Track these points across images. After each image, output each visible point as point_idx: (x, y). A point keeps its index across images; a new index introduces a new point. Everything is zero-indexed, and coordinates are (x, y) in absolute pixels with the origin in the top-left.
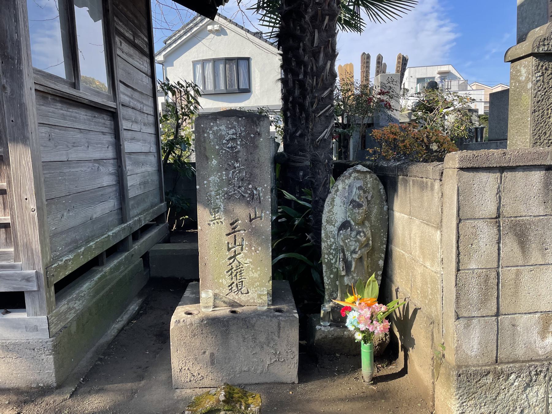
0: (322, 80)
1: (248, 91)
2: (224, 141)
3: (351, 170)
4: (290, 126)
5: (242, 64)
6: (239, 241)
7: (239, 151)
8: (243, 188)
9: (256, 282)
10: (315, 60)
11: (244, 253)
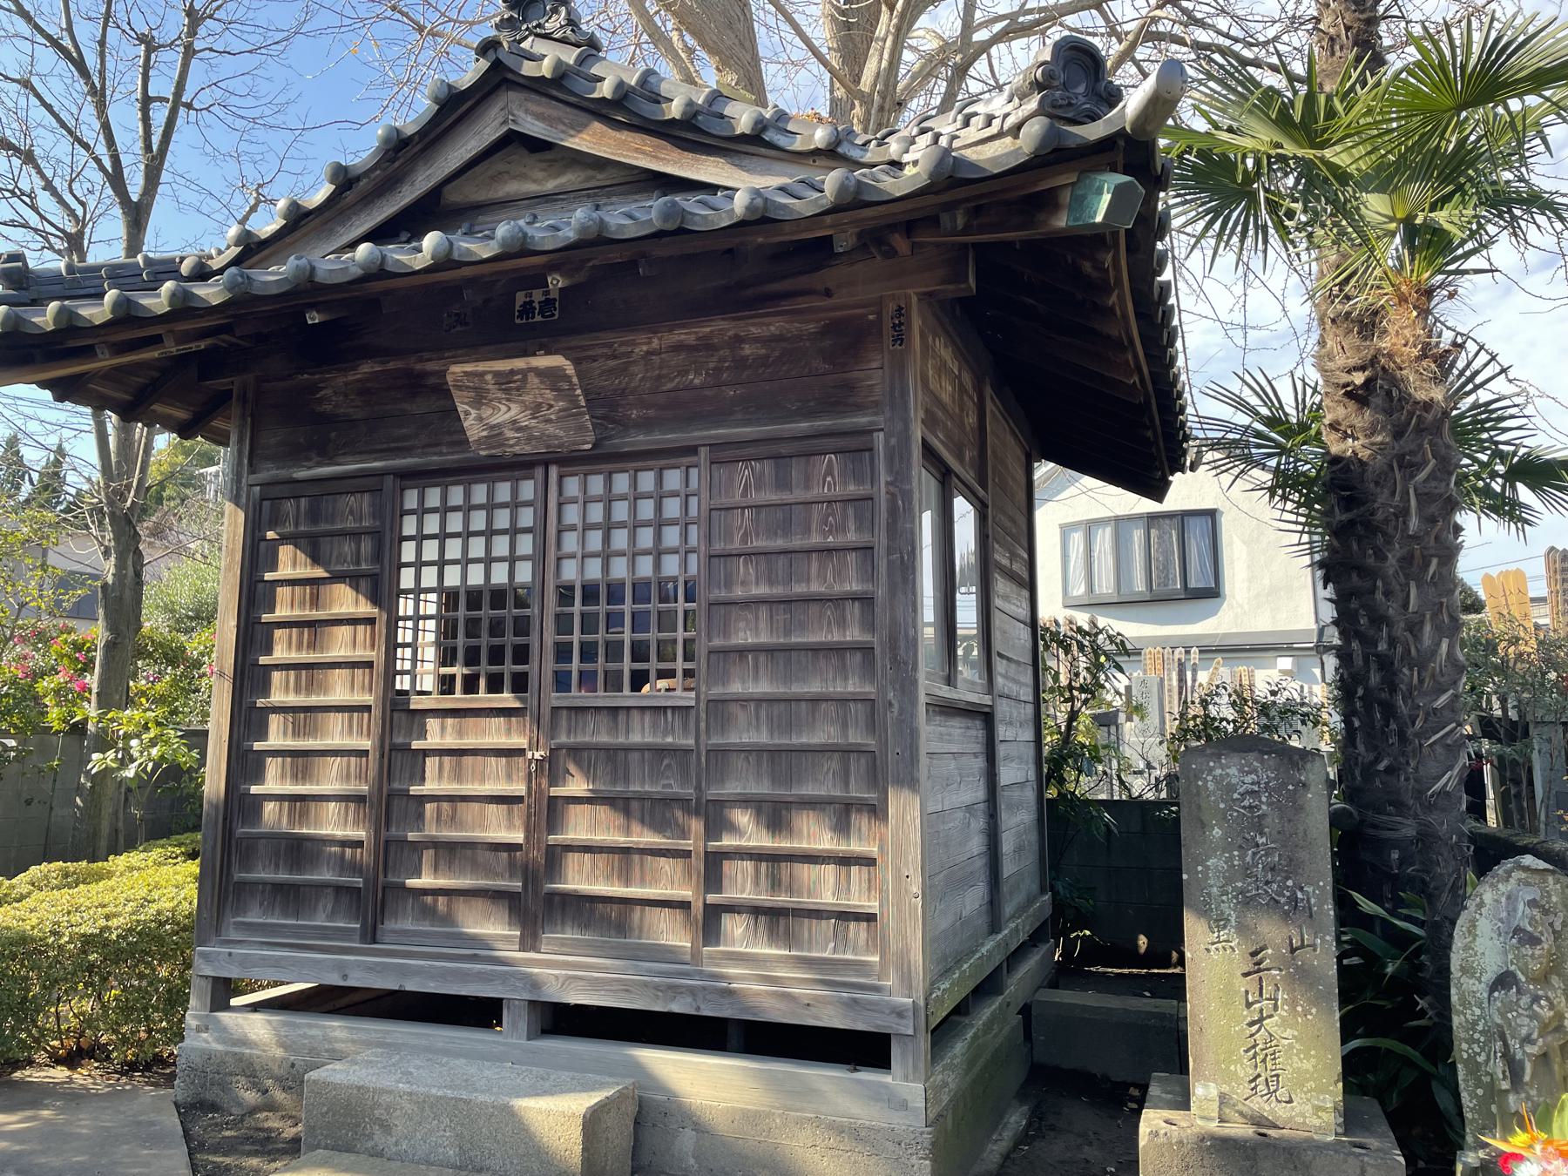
0: (1433, 676)
1: (1212, 593)
2: (1236, 796)
3: (1508, 864)
4: (1361, 748)
5: (1196, 528)
6: (1268, 990)
7: (1264, 815)
8: (1275, 886)
9: (1308, 1080)
10: (1415, 636)
11: (1281, 1017)
